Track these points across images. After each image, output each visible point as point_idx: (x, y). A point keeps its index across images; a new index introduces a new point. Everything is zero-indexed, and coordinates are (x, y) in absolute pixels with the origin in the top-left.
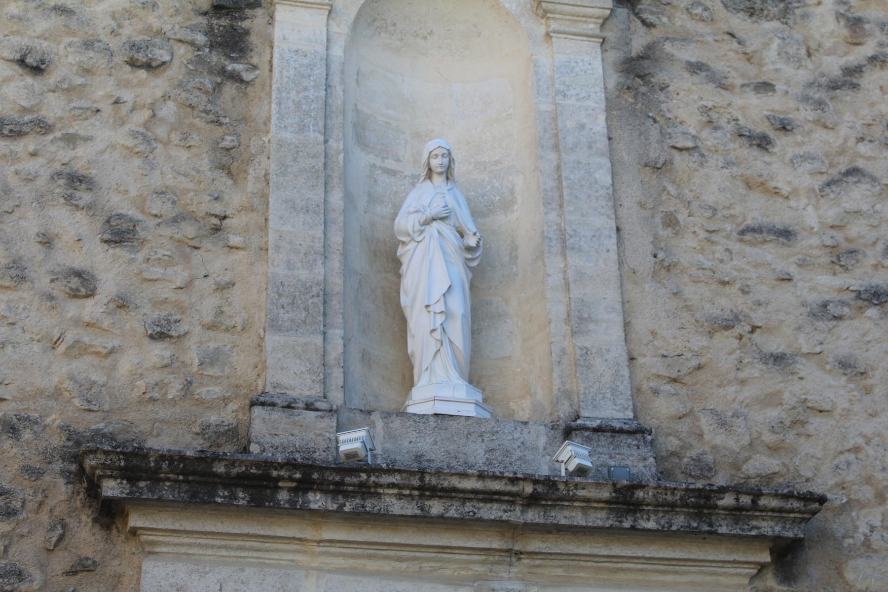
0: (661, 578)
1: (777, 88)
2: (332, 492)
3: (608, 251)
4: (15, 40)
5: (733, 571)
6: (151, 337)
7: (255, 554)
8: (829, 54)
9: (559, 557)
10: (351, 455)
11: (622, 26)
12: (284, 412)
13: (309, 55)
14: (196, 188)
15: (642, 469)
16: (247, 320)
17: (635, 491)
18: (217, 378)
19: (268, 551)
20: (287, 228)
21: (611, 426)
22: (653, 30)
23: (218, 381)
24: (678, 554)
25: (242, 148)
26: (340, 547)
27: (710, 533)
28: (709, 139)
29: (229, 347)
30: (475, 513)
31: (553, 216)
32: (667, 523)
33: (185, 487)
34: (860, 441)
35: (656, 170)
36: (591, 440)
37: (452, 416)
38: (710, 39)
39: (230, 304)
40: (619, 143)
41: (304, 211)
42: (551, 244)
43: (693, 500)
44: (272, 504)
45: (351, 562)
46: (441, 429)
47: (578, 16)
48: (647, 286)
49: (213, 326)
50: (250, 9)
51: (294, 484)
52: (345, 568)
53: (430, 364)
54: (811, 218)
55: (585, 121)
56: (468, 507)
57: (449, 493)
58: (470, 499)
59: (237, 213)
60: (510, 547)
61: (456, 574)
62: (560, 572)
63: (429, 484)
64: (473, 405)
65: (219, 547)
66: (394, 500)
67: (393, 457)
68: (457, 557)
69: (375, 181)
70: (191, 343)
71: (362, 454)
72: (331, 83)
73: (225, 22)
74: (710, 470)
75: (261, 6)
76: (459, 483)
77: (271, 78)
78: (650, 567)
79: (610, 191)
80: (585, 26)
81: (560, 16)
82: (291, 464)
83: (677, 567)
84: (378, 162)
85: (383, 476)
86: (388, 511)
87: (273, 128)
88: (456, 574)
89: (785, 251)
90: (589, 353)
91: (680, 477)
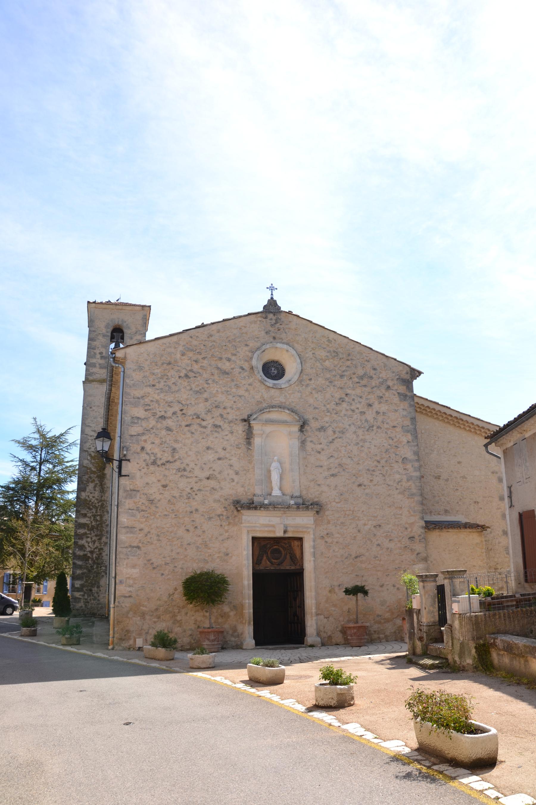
54: (325, 464)
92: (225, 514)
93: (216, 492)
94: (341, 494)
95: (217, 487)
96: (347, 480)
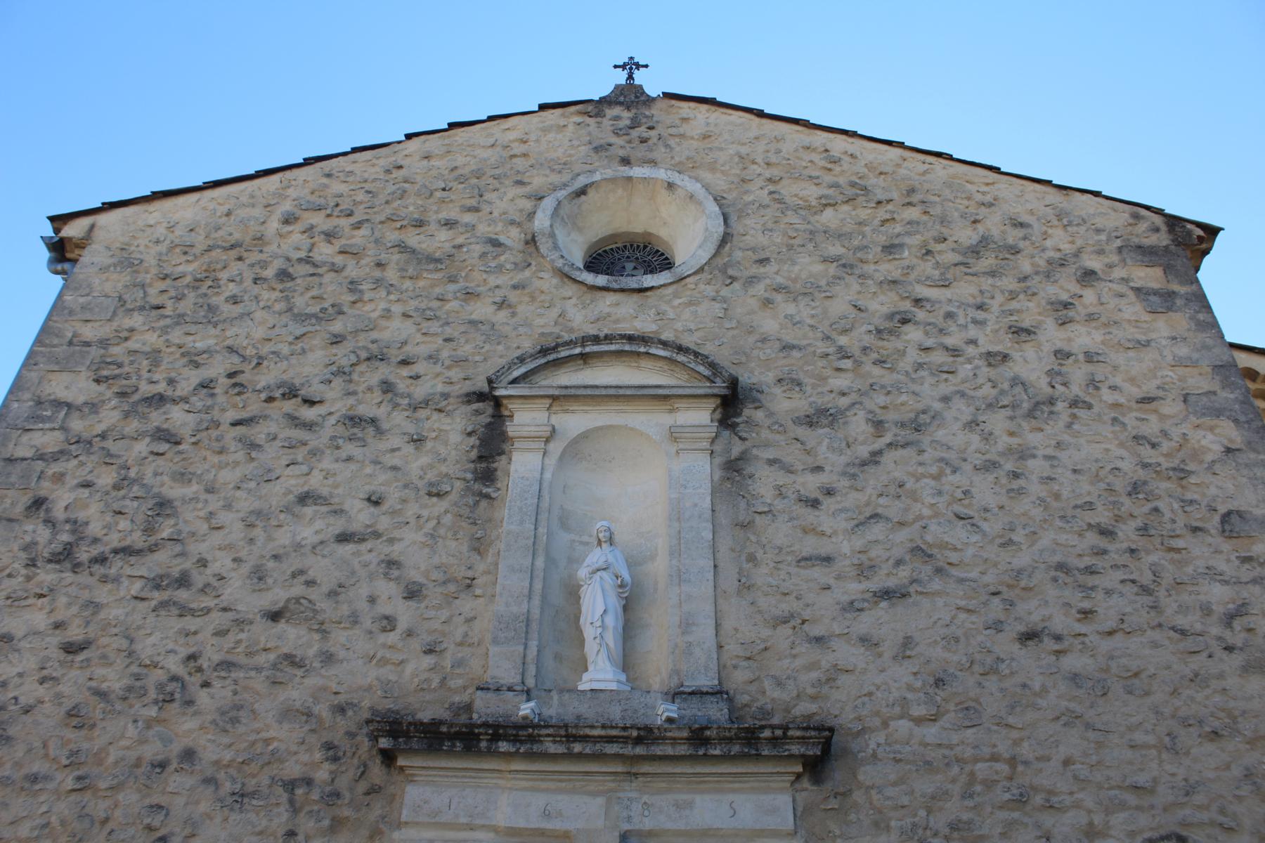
0: (731, 785)
1: (826, 468)
2: (513, 740)
4: (367, 488)
5: (779, 779)
6: (425, 652)
8: (862, 444)
10: (525, 718)
24: (740, 770)
27: (757, 755)
28: (779, 504)
31: (675, 562)
33: (425, 741)
34: (872, 688)
38: (783, 443)
45: (530, 784)
54: (846, 548)
56: (598, 746)
57: (585, 739)
62: (663, 785)
70: (448, 655)
71: (532, 716)
73: (484, 465)
74: (769, 714)
82: (486, 725)
84: (577, 538)
87: (505, 524)
89: (828, 570)
91: (749, 719)
92: (322, 774)
93: (300, 672)
94: (939, 682)
95: (311, 652)
96: (962, 616)
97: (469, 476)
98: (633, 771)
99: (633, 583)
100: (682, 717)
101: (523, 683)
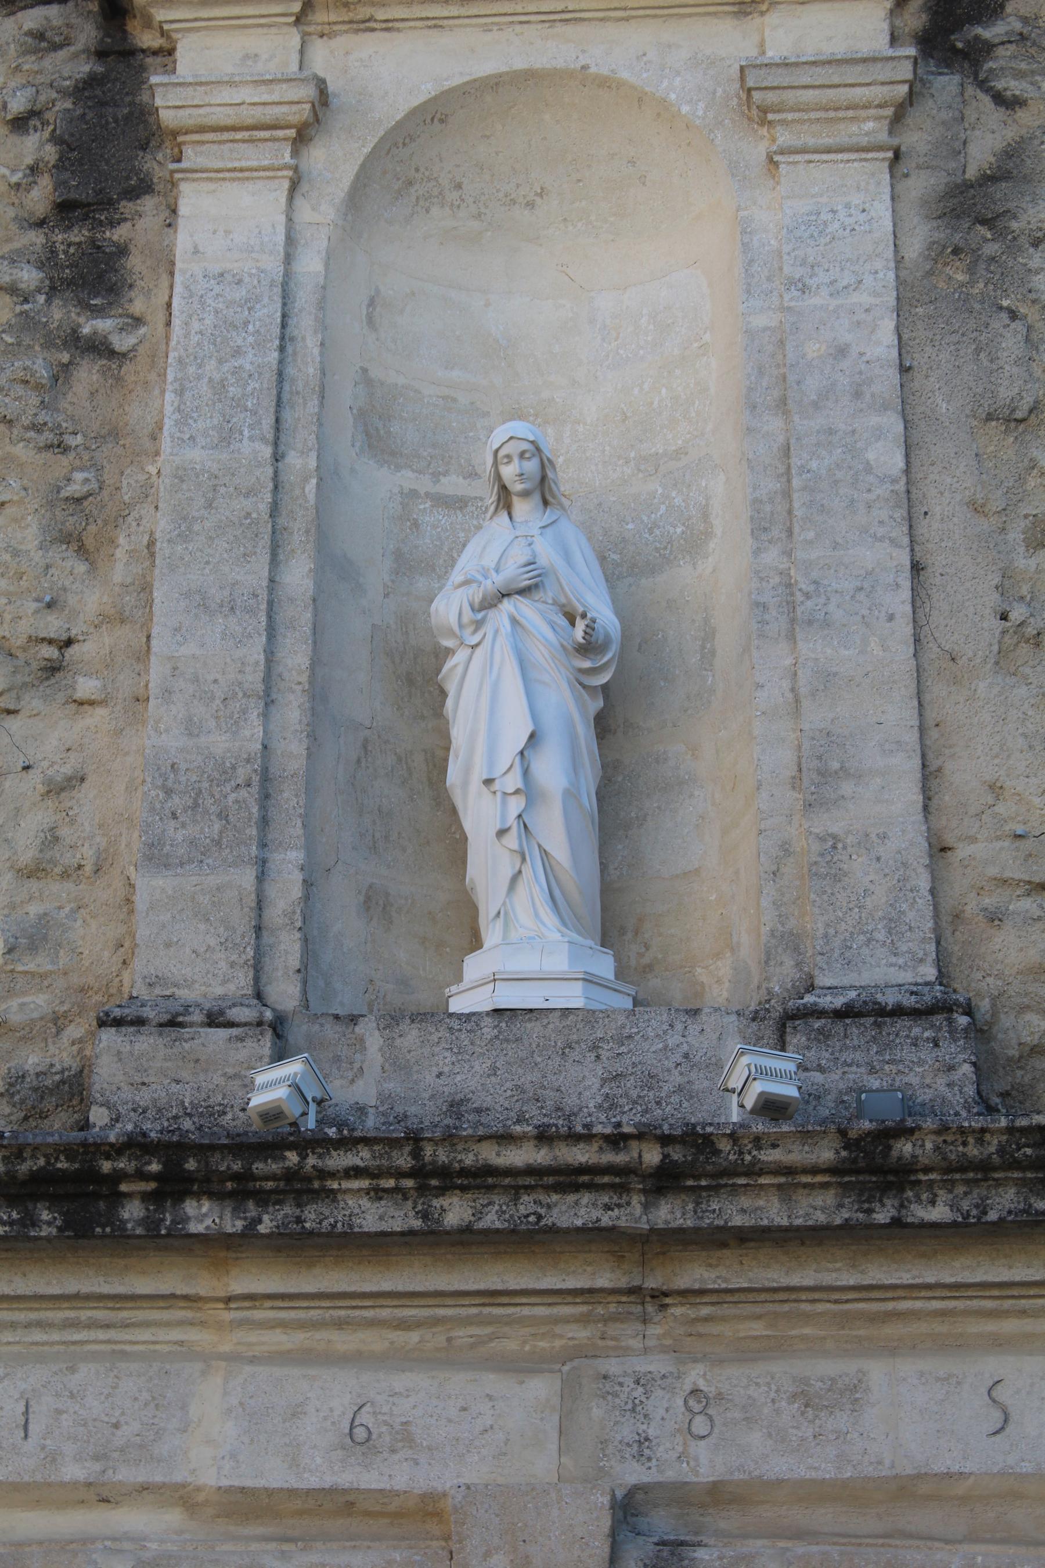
0: (991, 1326)
2: (231, 1195)
3: (891, 618)
7: (101, 1335)
9: (751, 1297)
10: (272, 1115)
11: (945, 115)
12: (161, 1035)
13: (247, 279)
14: (12, 588)
15: (943, 1089)
16: (106, 850)
17: (892, 1142)
18: (43, 976)
19: (127, 1326)
20: (190, 649)
21: (875, 1003)
22: (1021, 114)
23: (46, 983)
25: (105, 493)
26: (272, 1308)
29: (67, 909)
30: (540, 1217)
31: (772, 557)
32: (977, 1206)
35: (1013, 425)
36: (827, 1037)
37: (531, 1010)
39: (73, 822)
40: (927, 377)
41: (226, 610)
42: (767, 617)
43: (1029, 1151)
44: (108, 1230)
45: (299, 1338)
46: (507, 1041)
47: (836, 109)
48: (982, 686)
49: (38, 870)
50: (130, 200)
51: (152, 1186)
52: (289, 1352)
53: (504, 904)
55: (848, 337)
56: (527, 1204)
58: (529, 1189)
59: (92, 630)
60: (636, 1283)
61: (527, 1348)
62: (758, 1328)
63: (433, 1163)
64: (580, 984)
65: (28, 1326)
66: (365, 1202)
67: (400, 1109)
68: (526, 1311)
69: (416, 524)
71: (294, 1110)
72: (296, 333)
73: (78, 235)
75: (153, 191)
76: (498, 1155)
77: (168, 338)
78: (959, 1304)
79: (901, 486)
80: (854, 128)
81: (797, 115)
83: (1023, 1301)
84: (425, 484)
85: (334, 1153)
86: (351, 1226)
87: (166, 444)
88: (527, 1348)
90: (840, 846)
97: (29, 276)
98: (651, 1283)
99: (624, 636)
100: (812, 1096)
101: (259, 996)
